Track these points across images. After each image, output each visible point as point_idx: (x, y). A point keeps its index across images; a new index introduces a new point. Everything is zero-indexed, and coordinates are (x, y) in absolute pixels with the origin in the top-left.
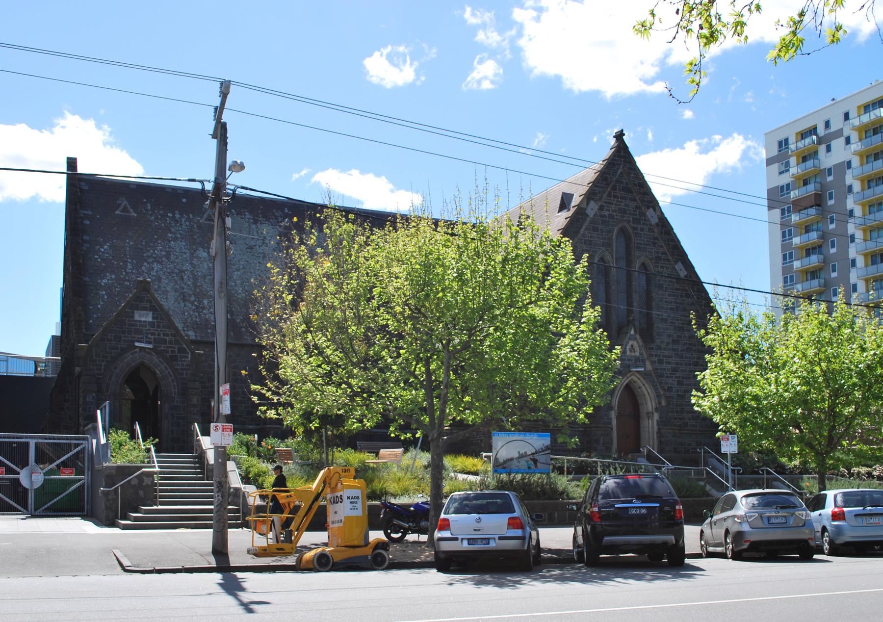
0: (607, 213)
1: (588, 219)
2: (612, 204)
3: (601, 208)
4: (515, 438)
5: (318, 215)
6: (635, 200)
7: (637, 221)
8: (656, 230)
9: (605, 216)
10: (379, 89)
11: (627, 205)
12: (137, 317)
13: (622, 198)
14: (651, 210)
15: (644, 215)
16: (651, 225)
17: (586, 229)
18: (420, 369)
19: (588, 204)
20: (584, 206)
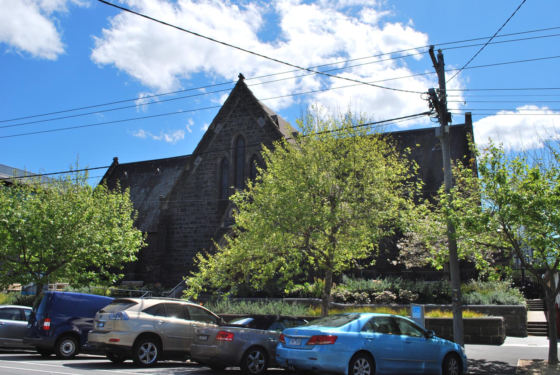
0: (229, 128)
1: (216, 136)
2: (233, 121)
3: (225, 126)
4: (535, 112)
5: (22, 256)
6: (249, 115)
7: (249, 128)
8: (264, 130)
9: (227, 131)
10: (545, 106)
11: (243, 120)
12: (225, 236)
13: (240, 116)
14: (261, 118)
15: (256, 123)
16: (260, 128)
17: (214, 142)
18: (314, 168)
19: (215, 127)
20: (213, 128)
